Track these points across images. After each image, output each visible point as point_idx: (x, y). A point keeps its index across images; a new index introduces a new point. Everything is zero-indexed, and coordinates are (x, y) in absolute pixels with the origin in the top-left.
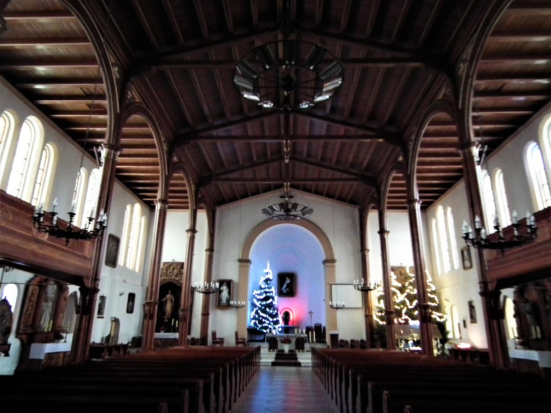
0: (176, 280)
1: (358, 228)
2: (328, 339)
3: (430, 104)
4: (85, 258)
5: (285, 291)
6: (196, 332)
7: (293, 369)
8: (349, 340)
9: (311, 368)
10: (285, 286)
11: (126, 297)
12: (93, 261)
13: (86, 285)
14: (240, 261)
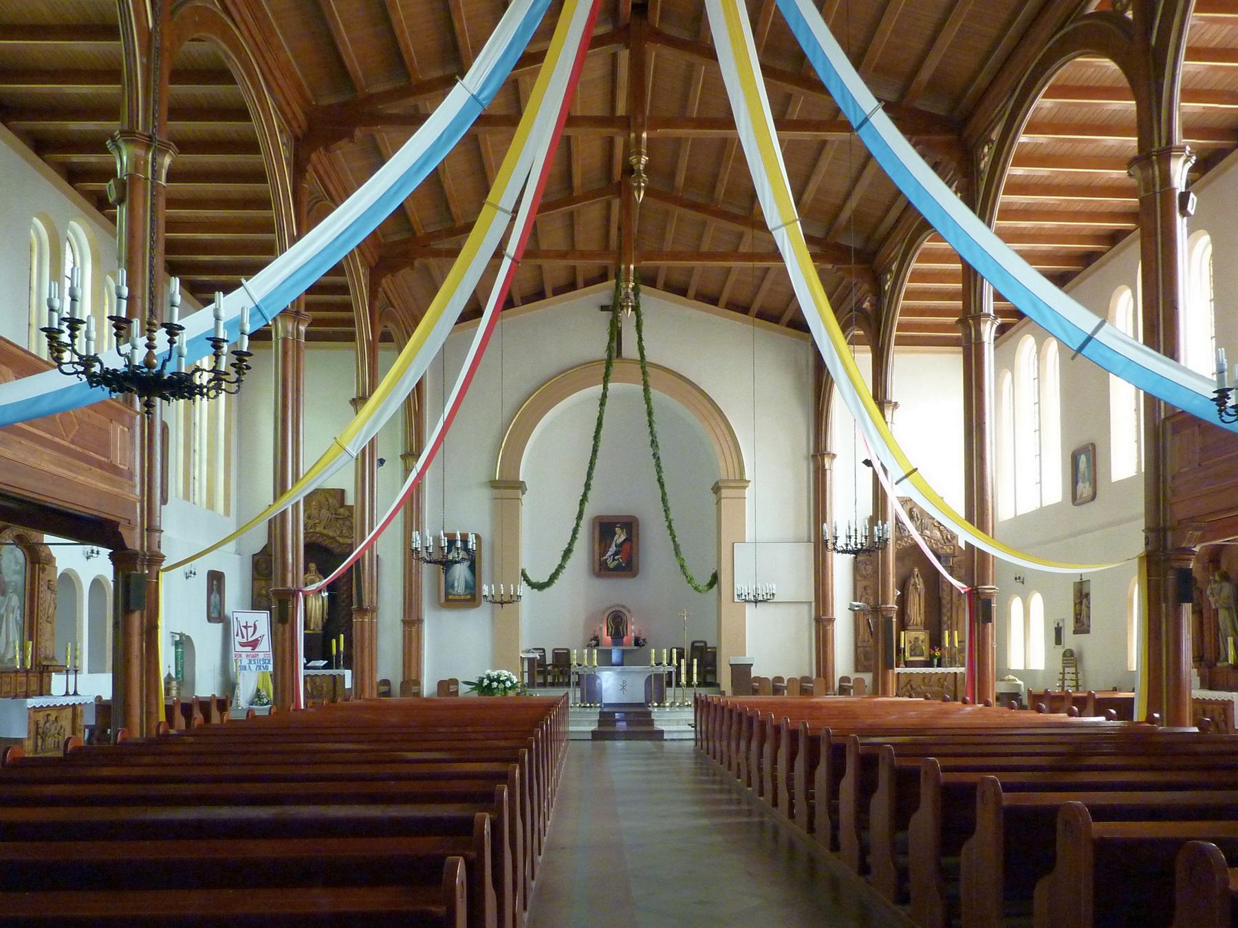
0: (328, 537)
1: (811, 399)
2: (725, 678)
3: (1061, 28)
4: (114, 469)
5: (612, 565)
6: (388, 666)
7: (648, 744)
8: (771, 679)
9: (693, 743)
10: (613, 549)
11: (201, 582)
12: (138, 479)
13: (129, 545)
14: (494, 485)
